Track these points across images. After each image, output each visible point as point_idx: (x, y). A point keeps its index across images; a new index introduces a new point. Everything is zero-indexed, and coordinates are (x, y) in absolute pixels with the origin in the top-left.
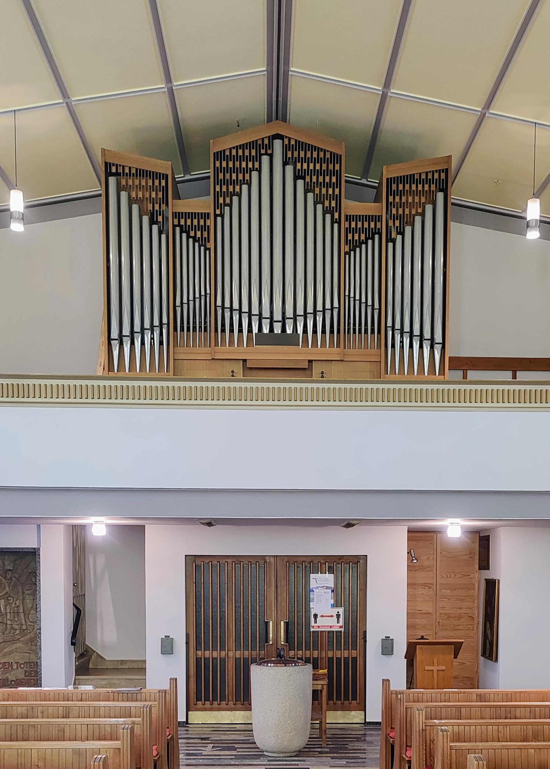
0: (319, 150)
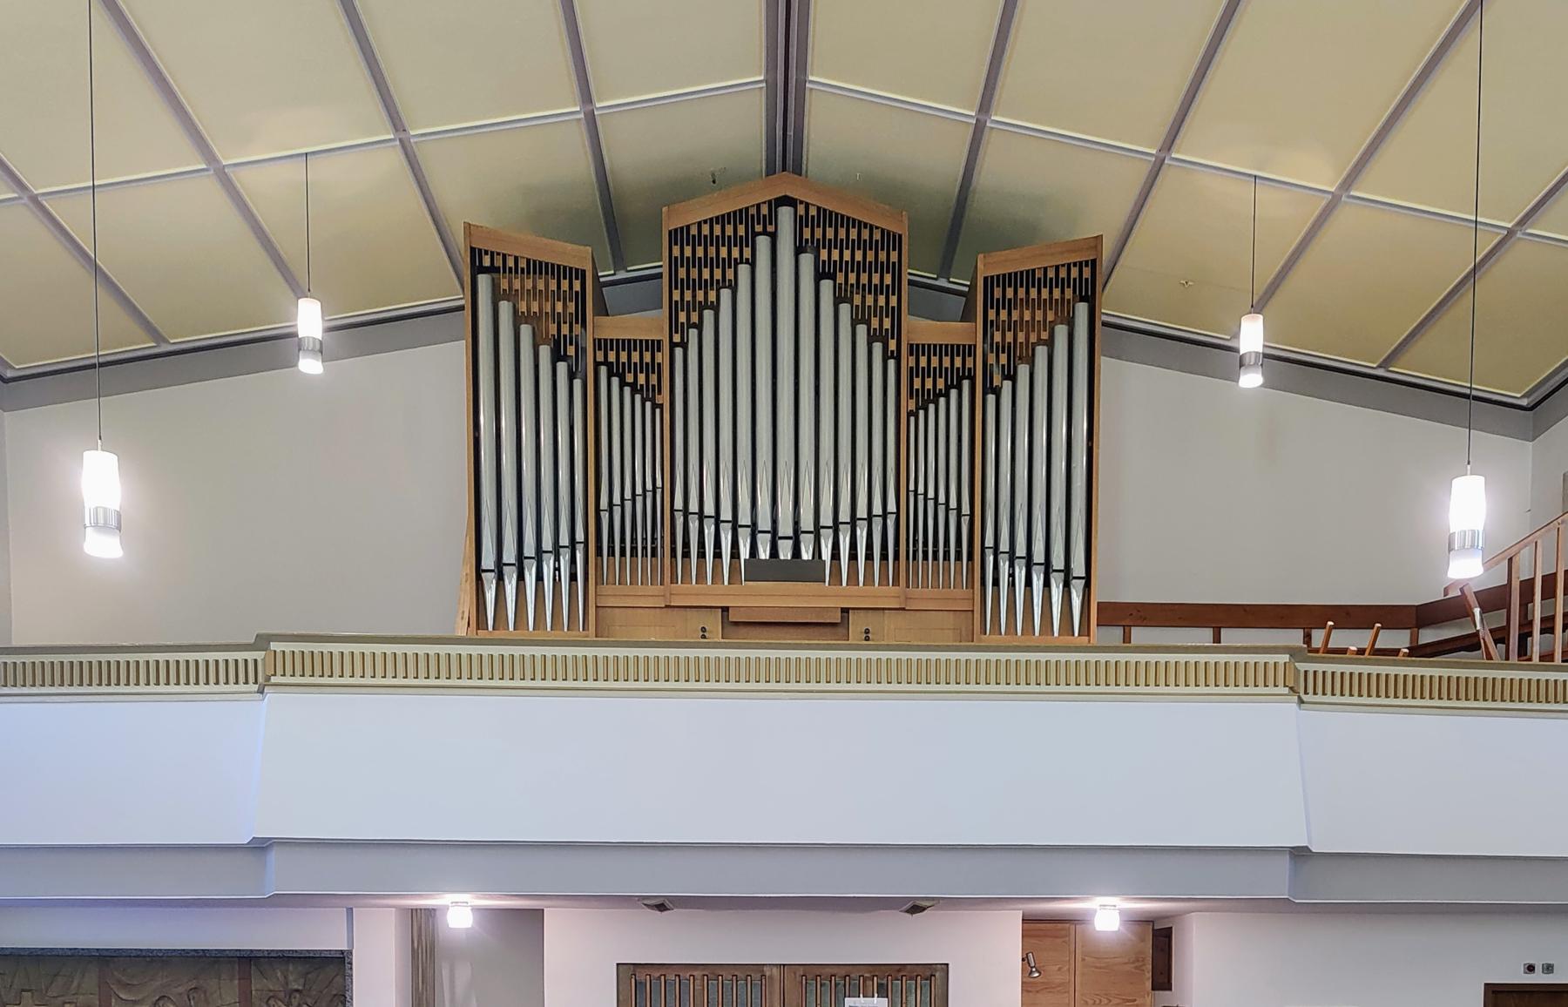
0: (861, 225)
